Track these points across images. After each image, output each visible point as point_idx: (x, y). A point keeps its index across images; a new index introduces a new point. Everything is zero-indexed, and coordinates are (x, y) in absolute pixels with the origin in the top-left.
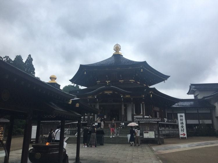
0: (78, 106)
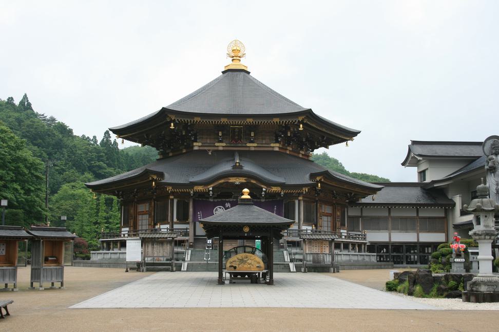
0: (2, 204)
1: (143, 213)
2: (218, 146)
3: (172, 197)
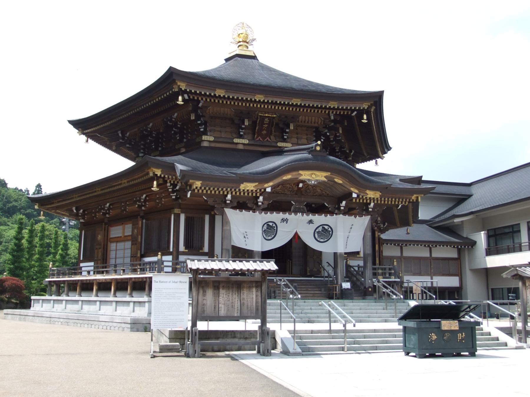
1: (118, 240)
2: (237, 144)
3: (177, 211)
